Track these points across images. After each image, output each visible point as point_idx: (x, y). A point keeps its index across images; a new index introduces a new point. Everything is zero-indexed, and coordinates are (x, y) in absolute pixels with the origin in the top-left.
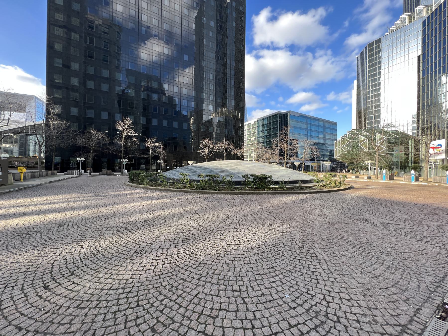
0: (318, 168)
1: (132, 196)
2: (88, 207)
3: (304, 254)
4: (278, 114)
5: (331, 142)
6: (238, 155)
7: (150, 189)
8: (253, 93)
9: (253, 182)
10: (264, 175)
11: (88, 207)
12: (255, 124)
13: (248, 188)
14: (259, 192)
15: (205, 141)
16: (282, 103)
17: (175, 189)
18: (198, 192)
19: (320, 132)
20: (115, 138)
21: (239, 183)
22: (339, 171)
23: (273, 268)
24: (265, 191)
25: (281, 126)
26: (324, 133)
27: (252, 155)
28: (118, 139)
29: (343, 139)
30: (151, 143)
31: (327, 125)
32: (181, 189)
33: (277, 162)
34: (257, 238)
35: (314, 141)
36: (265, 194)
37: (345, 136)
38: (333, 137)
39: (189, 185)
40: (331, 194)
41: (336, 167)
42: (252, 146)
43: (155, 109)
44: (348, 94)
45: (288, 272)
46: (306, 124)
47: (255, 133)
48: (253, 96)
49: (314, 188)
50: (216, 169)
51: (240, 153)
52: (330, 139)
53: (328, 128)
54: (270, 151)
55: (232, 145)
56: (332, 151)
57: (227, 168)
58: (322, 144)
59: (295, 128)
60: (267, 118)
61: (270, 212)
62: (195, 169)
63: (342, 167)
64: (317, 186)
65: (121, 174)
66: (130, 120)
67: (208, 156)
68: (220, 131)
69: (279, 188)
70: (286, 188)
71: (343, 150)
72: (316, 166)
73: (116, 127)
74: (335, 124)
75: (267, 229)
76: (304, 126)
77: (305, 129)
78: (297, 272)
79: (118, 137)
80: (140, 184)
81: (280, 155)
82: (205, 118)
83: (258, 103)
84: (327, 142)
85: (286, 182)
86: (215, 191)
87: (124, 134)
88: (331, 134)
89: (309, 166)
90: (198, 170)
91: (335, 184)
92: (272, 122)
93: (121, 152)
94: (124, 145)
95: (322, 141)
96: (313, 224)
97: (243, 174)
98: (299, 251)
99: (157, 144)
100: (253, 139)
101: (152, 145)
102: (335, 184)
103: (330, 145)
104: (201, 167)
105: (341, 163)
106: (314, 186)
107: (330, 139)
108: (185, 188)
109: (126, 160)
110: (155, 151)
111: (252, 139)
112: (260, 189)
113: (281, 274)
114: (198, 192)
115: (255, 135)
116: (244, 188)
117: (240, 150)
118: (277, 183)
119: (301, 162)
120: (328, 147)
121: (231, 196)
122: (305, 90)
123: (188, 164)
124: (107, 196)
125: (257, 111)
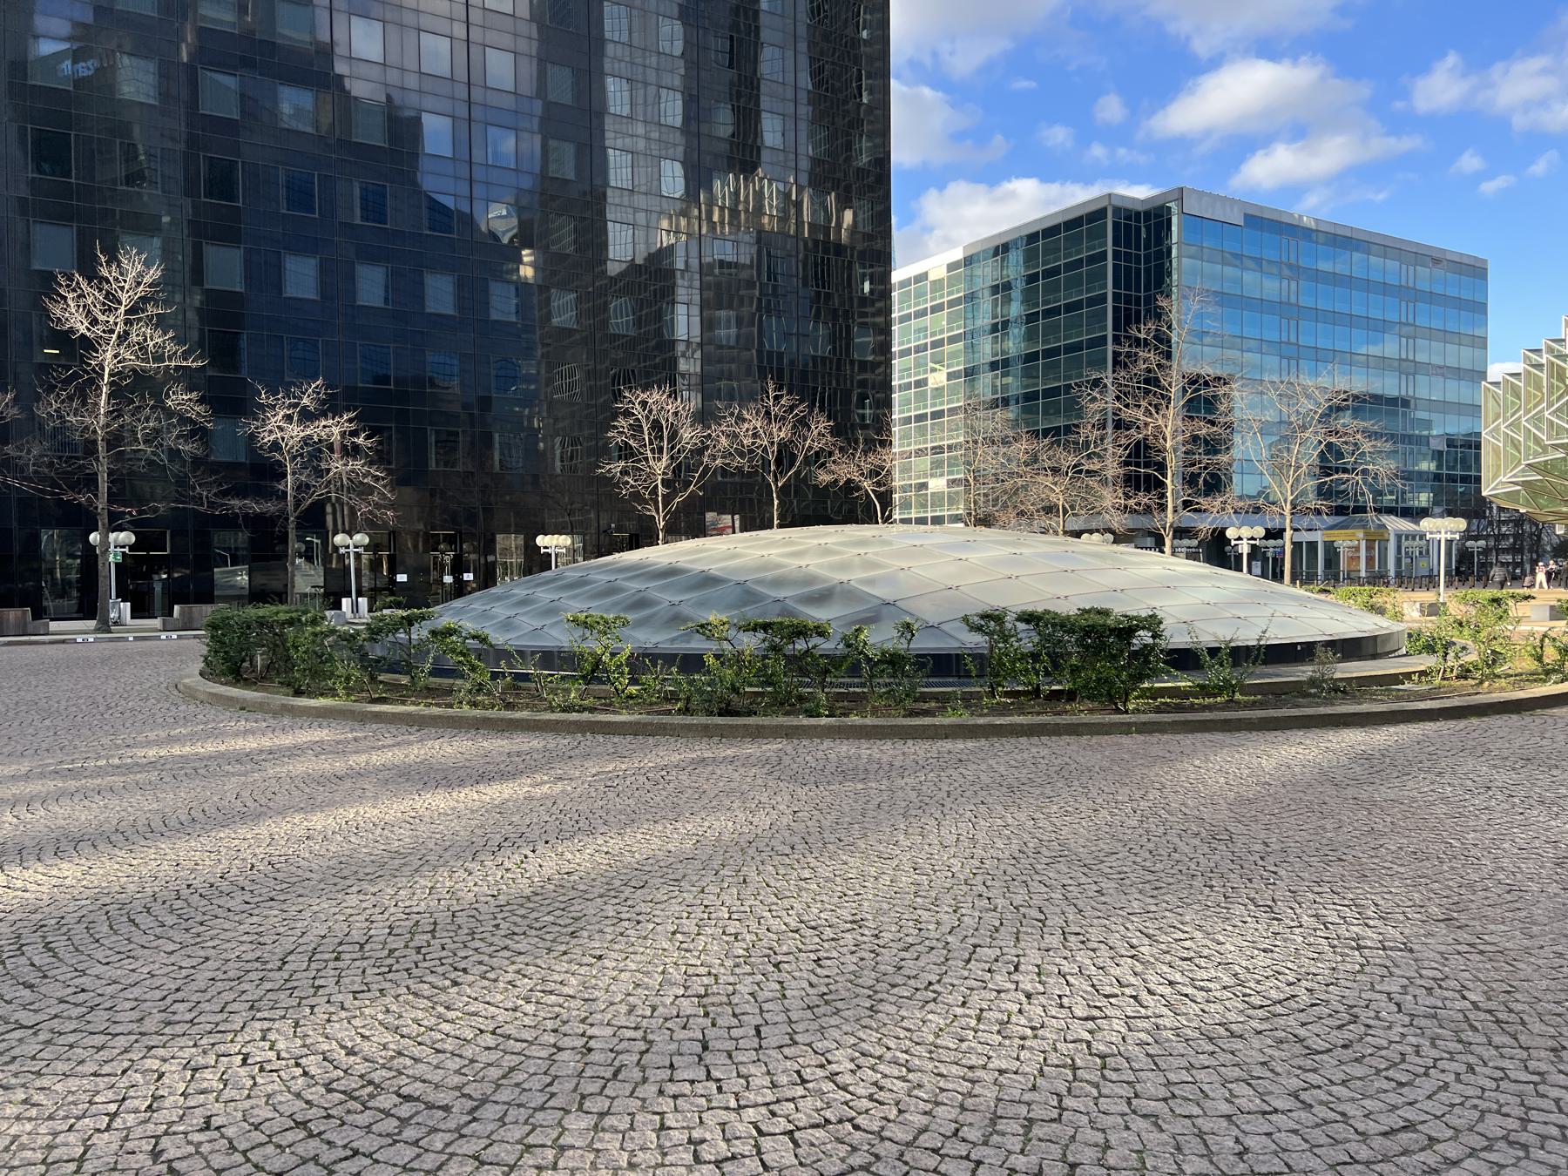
0: (1370, 560)
1: (300, 767)
2: (76, 843)
3: (1543, 1054)
4: (1097, 215)
5: (1454, 391)
6: (858, 488)
7: (378, 717)
8: (935, 76)
9: (1035, 657)
10: (1105, 613)
11: (76, 843)
12: (952, 281)
13: (1007, 695)
14: (1085, 718)
15: (644, 404)
16: (1118, 136)
17: (554, 716)
18: (706, 732)
19: (1380, 327)
20: (51, 389)
21: (944, 665)
22: (1497, 573)
23: (1410, 1126)
24: (1118, 711)
25: (1128, 288)
26: (1410, 331)
27: (937, 484)
28: (70, 398)
29: (1539, 366)
30: (289, 418)
31: (1423, 277)
32: (586, 716)
33: (1115, 526)
34: (1227, 980)
35: (1342, 383)
36: (1126, 729)
37: (1550, 350)
38: (1457, 355)
39: (633, 689)
40: (1527, 719)
41: (1486, 552)
42: (922, 431)
43: (300, 195)
44: (1544, 71)
45: (1502, 1145)
46: (1286, 272)
47: (952, 340)
48: (927, 92)
49: (1407, 686)
50: (778, 583)
51: (875, 473)
52: (1445, 371)
53: (1432, 298)
54: (1068, 460)
55: (820, 425)
56: (1470, 447)
57: (844, 578)
58: (1393, 401)
59: (1227, 299)
60: (1033, 238)
61: (1217, 836)
62: (635, 586)
63: (1520, 551)
64: (1422, 673)
65: (97, 630)
66: (147, 264)
67: (667, 500)
68: (733, 331)
69: (1204, 690)
70: (1245, 690)
71: (1537, 441)
72: (1357, 549)
73: (46, 313)
74: (1476, 271)
75: (1259, 929)
76: (1271, 288)
77: (1284, 309)
78: (1550, 1145)
79: (67, 381)
80: (298, 693)
81: (1133, 482)
82: (622, 247)
83: (958, 137)
84: (1425, 389)
85: (1240, 655)
86: (813, 721)
87: (108, 358)
88: (1446, 336)
89: (1312, 546)
90: (663, 588)
91: (1539, 659)
92: (1069, 266)
93: (91, 482)
94: (114, 440)
95: (1389, 386)
96: (1508, 897)
97: (973, 610)
98: (1507, 1040)
99: (333, 429)
100: (938, 379)
101: (295, 432)
102: (1539, 659)
103: (1445, 407)
104: (670, 572)
105: (1519, 521)
106: (1408, 676)
107: (1445, 371)
108: (608, 707)
109: (126, 537)
110: (320, 473)
111: (931, 384)
112: (1091, 698)
113: (1470, 1155)
114: (706, 727)
115: (953, 355)
116: (978, 696)
117: (871, 458)
118: (1185, 659)
119: (1275, 524)
120: (1428, 424)
121: (918, 749)
122: (1267, 48)
123: (537, 562)
124: (129, 769)
125: (958, 189)
